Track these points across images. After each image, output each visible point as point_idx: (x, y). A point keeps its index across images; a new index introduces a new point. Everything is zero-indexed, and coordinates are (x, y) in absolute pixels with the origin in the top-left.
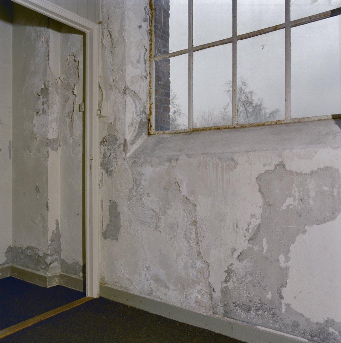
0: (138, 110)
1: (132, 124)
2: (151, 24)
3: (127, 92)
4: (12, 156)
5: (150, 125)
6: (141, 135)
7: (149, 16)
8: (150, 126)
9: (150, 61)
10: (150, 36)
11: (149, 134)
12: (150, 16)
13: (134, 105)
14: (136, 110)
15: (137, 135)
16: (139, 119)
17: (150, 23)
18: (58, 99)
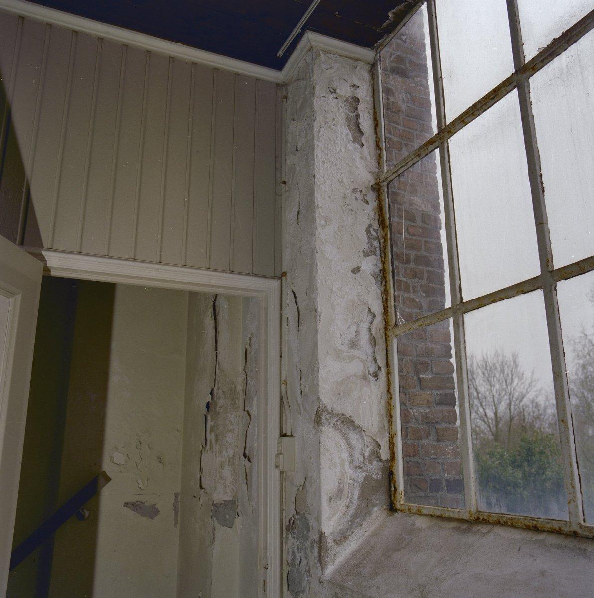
0: (357, 455)
1: (340, 492)
2: (385, 258)
3: (324, 418)
4: (179, 522)
5: (392, 485)
6: (369, 513)
7: (380, 243)
8: (393, 489)
9: (387, 337)
10: (384, 283)
11: (392, 508)
12: (382, 241)
13: (344, 446)
14: (351, 456)
15: (355, 516)
16: (360, 476)
17: (383, 256)
18: (237, 419)
